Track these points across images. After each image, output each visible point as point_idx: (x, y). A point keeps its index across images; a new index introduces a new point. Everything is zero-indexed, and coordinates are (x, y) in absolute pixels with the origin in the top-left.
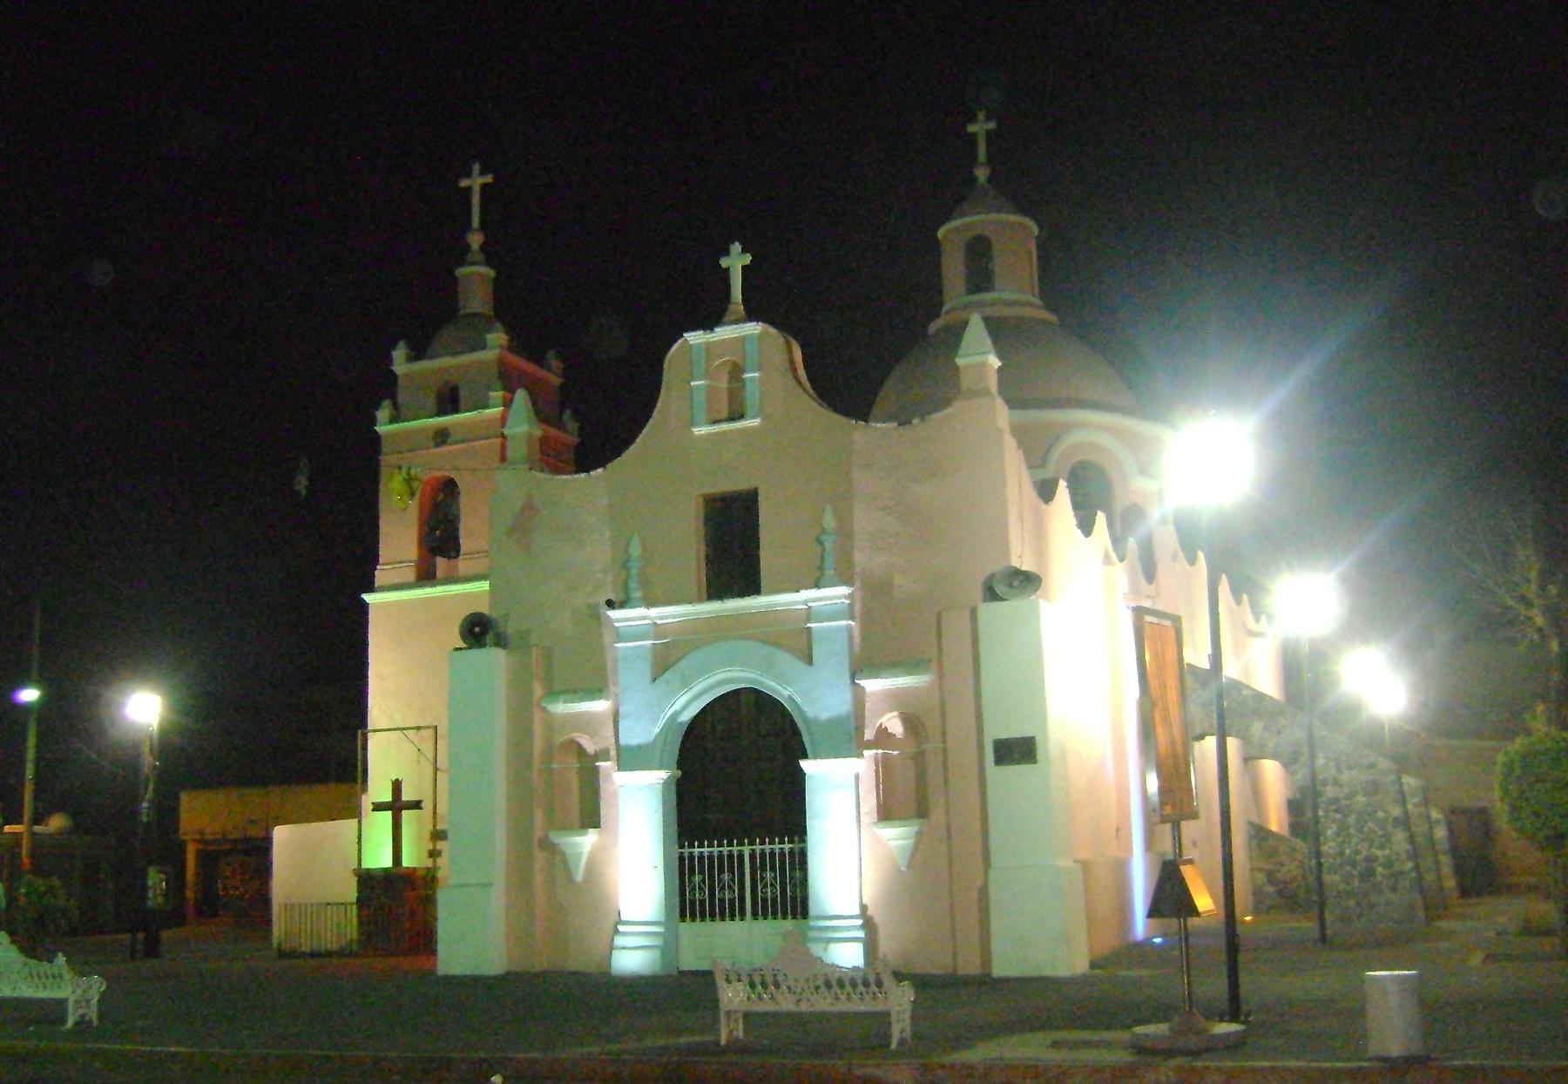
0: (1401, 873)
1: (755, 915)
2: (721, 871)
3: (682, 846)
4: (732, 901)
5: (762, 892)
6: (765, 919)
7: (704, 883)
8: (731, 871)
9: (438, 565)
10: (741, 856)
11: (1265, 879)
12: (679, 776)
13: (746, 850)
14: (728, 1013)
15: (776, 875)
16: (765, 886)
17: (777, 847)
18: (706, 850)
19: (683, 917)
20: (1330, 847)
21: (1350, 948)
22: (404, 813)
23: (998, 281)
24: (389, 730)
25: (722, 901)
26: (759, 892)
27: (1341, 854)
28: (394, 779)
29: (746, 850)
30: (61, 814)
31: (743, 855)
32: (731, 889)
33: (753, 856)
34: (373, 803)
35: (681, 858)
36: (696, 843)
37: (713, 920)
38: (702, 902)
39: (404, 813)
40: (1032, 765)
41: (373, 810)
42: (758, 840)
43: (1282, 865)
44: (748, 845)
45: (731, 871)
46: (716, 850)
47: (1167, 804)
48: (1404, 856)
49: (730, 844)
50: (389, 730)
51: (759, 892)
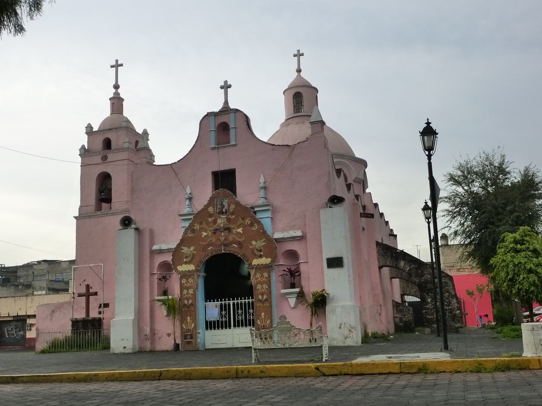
1: (235, 326)
4: (226, 322)
5: (248, 317)
6: (215, 329)
8: (225, 310)
10: (229, 305)
11: (399, 321)
14: (442, 336)
16: (239, 315)
17: (239, 301)
18: (247, 301)
19: (207, 328)
20: (429, 306)
21: (179, 380)
22: (91, 297)
26: (244, 316)
28: (86, 284)
29: (231, 302)
30: (242, 274)
33: (234, 304)
34: (78, 294)
36: (231, 299)
37: (211, 329)
38: (242, 321)
39: (91, 297)
40: (329, 257)
41: (78, 296)
43: (405, 315)
45: (225, 310)
47: (14, 318)
48: (456, 308)
51: (244, 316)
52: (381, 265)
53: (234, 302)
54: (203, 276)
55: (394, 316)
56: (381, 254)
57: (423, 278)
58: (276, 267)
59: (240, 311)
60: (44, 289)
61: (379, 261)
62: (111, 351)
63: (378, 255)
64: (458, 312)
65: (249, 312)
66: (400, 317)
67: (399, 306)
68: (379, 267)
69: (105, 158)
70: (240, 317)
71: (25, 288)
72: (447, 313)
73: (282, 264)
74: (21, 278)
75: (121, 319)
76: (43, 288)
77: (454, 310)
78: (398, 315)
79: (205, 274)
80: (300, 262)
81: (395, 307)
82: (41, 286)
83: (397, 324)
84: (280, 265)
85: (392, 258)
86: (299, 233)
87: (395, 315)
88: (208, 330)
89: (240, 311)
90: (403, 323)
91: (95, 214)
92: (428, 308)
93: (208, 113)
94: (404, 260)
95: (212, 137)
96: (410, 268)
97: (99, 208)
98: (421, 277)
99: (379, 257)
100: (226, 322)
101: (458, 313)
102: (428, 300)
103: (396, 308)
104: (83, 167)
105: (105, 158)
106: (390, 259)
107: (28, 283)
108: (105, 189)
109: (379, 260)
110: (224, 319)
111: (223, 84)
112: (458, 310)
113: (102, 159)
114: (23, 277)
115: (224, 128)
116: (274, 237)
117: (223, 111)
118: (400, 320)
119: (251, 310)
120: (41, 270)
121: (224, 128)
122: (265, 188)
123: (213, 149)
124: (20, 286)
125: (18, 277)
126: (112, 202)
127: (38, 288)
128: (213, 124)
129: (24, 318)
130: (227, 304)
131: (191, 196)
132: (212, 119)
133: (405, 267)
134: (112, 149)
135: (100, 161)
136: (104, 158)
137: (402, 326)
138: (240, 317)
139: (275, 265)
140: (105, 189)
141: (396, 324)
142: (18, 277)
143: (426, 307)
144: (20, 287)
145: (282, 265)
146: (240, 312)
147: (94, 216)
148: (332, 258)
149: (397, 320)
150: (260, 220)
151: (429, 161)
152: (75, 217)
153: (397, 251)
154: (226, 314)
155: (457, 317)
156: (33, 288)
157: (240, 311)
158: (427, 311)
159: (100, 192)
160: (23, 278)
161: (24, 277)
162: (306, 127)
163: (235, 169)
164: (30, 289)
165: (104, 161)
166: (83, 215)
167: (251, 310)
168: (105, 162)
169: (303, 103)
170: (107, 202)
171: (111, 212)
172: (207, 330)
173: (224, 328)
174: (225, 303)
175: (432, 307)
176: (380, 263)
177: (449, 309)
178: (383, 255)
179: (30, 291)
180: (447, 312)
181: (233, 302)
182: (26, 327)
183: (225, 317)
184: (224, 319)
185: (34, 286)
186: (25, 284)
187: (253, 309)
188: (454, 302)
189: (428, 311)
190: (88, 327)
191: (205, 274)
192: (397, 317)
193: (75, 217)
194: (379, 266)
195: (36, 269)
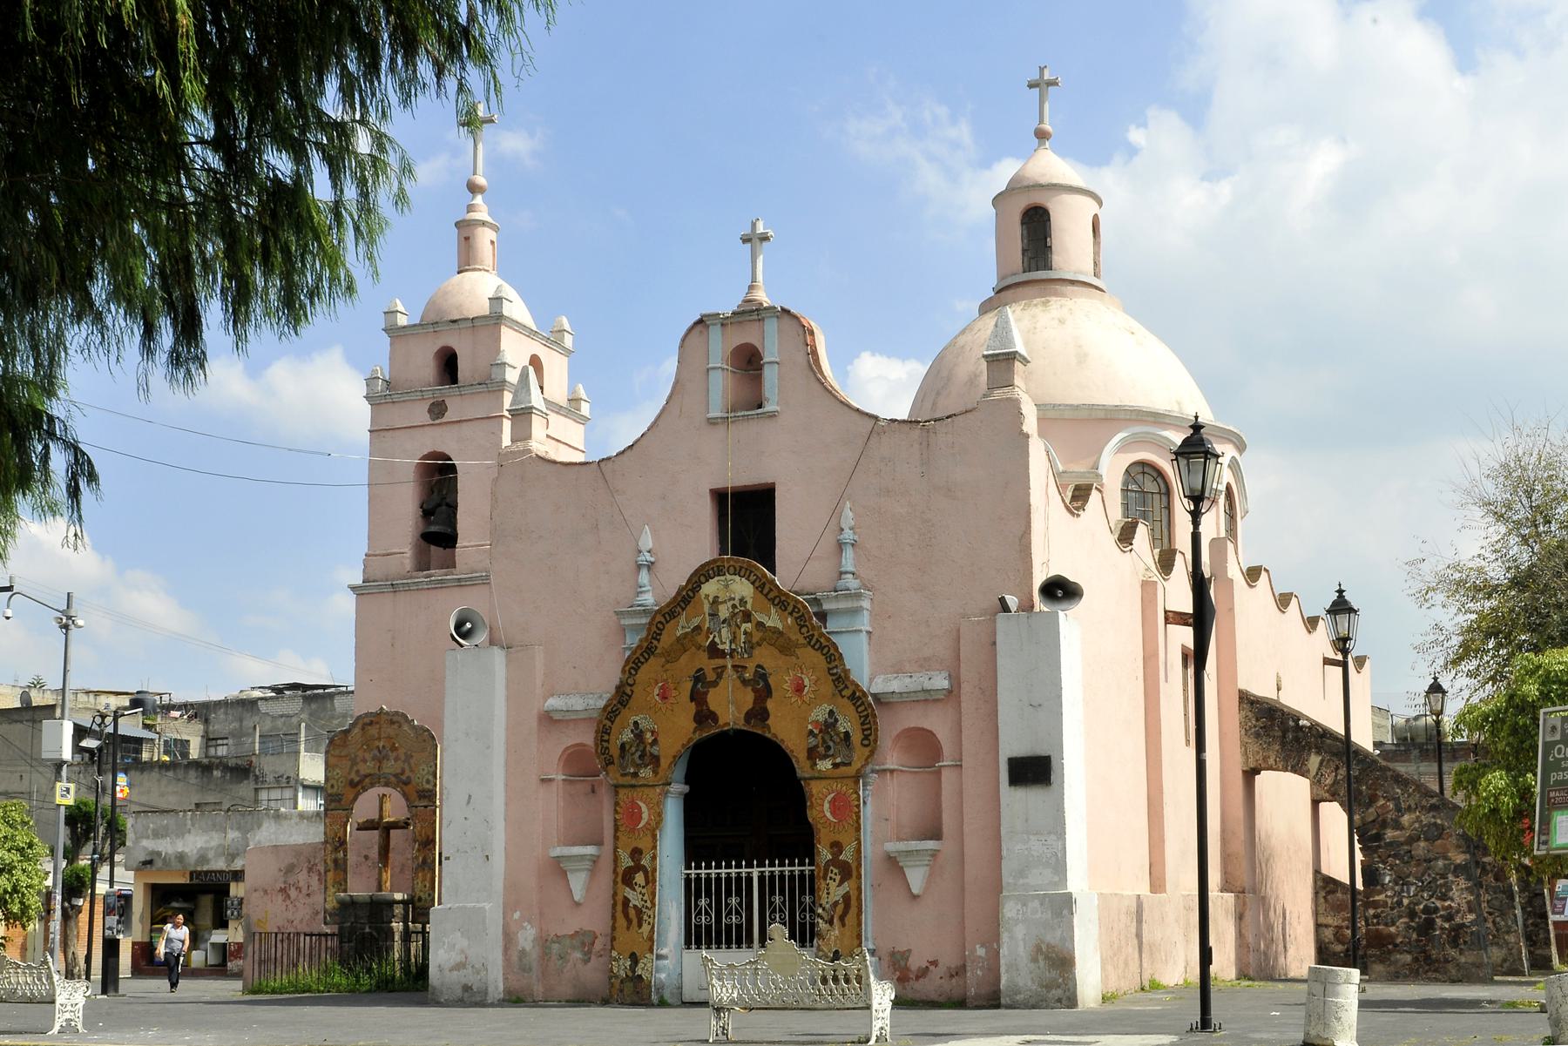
0: (1463, 926)
2: (729, 894)
3: (688, 867)
4: (739, 927)
7: (741, 906)
8: (739, 894)
9: (432, 552)
10: (749, 879)
11: (1332, 937)
12: (688, 791)
13: (755, 872)
15: (785, 898)
19: (688, 944)
20: (1386, 896)
23: (412, 469)
24: (1272, 589)
25: (729, 927)
27: (1400, 903)
29: (755, 872)
31: (752, 878)
32: (738, 913)
33: (761, 878)
35: (688, 880)
41: (358, 829)
42: (797, 861)
44: (757, 867)
45: (739, 894)
46: (797, 869)
48: (1464, 907)
49: (782, 864)
50: (1272, 589)
52: (1252, 766)
53: (762, 872)
54: (680, 793)
55: (1319, 923)
56: (1253, 730)
57: (1371, 810)
58: (876, 775)
59: (777, 898)
60: (288, 783)
61: (1245, 754)
62: (1080, 1007)
63: (1243, 732)
64: (1471, 917)
65: (801, 903)
66: (1336, 927)
67: (1333, 892)
68: (1245, 772)
69: (438, 409)
70: (778, 916)
71: (231, 777)
72: (1437, 920)
73: (892, 767)
74: (220, 742)
75: (458, 907)
76: (284, 780)
77: (1458, 911)
78: (1330, 921)
79: (686, 789)
80: (940, 764)
81: (1323, 894)
82: (280, 774)
83: (1327, 948)
84: (885, 770)
85: (1283, 744)
86: (941, 682)
87: (1322, 920)
88: (691, 949)
89: (777, 898)
90: (1343, 944)
91: (409, 581)
92: (1381, 903)
93: (703, 316)
94: (1318, 753)
95: (720, 387)
96: (1336, 776)
97: (423, 564)
98: (1369, 805)
99: (1246, 740)
100: (739, 927)
101: (1469, 920)
102: (1384, 879)
103: (1325, 898)
104: (376, 434)
105: (438, 409)
106: (1277, 747)
107: (240, 762)
108: (439, 505)
109: (1246, 750)
110: (734, 918)
111: (748, 231)
112: (1470, 911)
113: (430, 411)
114: (227, 738)
115: (749, 361)
116: (874, 690)
117: (743, 312)
118: (1335, 935)
119: (807, 898)
120: (282, 716)
121: (749, 361)
122: (853, 545)
123: (712, 422)
124: (217, 768)
125: (213, 739)
126: (457, 545)
127: (270, 778)
128: (719, 347)
129: (223, 880)
130: (723, 876)
131: (652, 559)
132: (715, 333)
133: (1322, 775)
134: (459, 384)
135: (426, 419)
136: (436, 411)
137: (1342, 955)
138: (778, 916)
139: (873, 771)
140: (439, 505)
141: (1323, 946)
142: (213, 739)
143: (1377, 898)
144: (217, 773)
145: (892, 771)
146: (777, 901)
147: (407, 588)
148: (1022, 758)
149: (1328, 934)
150: (834, 638)
151: (1194, 529)
152: (353, 588)
153: (1301, 723)
154: (740, 904)
155: (1466, 932)
156: (257, 777)
157: (777, 899)
158: (1379, 911)
159: (423, 511)
160: (225, 742)
161: (230, 741)
162: (1053, 319)
163: (774, 483)
164: (245, 782)
165: (438, 418)
166: (374, 582)
167: (807, 898)
168: (437, 422)
169: (1048, 239)
170: (444, 544)
171: (455, 577)
172: (689, 948)
173: (734, 946)
174: (739, 873)
175: (1395, 900)
176: (1248, 758)
177: (1445, 908)
178: (1257, 735)
179: (245, 789)
180: (1437, 917)
181: (759, 872)
182: (227, 908)
183: (781, 910)
184: (734, 918)
185: (257, 773)
186: (232, 763)
187: (812, 892)
188: (1460, 887)
189: (1382, 912)
190: (383, 923)
191: (686, 789)
192: (1327, 926)
193: (353, 588)
194: (1245, 769)
195: (267, 713)
